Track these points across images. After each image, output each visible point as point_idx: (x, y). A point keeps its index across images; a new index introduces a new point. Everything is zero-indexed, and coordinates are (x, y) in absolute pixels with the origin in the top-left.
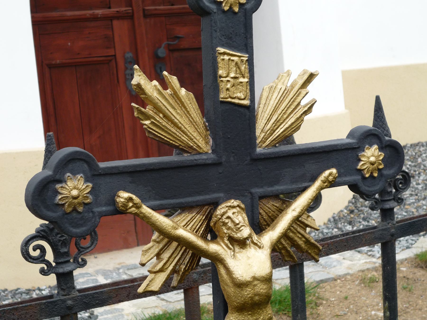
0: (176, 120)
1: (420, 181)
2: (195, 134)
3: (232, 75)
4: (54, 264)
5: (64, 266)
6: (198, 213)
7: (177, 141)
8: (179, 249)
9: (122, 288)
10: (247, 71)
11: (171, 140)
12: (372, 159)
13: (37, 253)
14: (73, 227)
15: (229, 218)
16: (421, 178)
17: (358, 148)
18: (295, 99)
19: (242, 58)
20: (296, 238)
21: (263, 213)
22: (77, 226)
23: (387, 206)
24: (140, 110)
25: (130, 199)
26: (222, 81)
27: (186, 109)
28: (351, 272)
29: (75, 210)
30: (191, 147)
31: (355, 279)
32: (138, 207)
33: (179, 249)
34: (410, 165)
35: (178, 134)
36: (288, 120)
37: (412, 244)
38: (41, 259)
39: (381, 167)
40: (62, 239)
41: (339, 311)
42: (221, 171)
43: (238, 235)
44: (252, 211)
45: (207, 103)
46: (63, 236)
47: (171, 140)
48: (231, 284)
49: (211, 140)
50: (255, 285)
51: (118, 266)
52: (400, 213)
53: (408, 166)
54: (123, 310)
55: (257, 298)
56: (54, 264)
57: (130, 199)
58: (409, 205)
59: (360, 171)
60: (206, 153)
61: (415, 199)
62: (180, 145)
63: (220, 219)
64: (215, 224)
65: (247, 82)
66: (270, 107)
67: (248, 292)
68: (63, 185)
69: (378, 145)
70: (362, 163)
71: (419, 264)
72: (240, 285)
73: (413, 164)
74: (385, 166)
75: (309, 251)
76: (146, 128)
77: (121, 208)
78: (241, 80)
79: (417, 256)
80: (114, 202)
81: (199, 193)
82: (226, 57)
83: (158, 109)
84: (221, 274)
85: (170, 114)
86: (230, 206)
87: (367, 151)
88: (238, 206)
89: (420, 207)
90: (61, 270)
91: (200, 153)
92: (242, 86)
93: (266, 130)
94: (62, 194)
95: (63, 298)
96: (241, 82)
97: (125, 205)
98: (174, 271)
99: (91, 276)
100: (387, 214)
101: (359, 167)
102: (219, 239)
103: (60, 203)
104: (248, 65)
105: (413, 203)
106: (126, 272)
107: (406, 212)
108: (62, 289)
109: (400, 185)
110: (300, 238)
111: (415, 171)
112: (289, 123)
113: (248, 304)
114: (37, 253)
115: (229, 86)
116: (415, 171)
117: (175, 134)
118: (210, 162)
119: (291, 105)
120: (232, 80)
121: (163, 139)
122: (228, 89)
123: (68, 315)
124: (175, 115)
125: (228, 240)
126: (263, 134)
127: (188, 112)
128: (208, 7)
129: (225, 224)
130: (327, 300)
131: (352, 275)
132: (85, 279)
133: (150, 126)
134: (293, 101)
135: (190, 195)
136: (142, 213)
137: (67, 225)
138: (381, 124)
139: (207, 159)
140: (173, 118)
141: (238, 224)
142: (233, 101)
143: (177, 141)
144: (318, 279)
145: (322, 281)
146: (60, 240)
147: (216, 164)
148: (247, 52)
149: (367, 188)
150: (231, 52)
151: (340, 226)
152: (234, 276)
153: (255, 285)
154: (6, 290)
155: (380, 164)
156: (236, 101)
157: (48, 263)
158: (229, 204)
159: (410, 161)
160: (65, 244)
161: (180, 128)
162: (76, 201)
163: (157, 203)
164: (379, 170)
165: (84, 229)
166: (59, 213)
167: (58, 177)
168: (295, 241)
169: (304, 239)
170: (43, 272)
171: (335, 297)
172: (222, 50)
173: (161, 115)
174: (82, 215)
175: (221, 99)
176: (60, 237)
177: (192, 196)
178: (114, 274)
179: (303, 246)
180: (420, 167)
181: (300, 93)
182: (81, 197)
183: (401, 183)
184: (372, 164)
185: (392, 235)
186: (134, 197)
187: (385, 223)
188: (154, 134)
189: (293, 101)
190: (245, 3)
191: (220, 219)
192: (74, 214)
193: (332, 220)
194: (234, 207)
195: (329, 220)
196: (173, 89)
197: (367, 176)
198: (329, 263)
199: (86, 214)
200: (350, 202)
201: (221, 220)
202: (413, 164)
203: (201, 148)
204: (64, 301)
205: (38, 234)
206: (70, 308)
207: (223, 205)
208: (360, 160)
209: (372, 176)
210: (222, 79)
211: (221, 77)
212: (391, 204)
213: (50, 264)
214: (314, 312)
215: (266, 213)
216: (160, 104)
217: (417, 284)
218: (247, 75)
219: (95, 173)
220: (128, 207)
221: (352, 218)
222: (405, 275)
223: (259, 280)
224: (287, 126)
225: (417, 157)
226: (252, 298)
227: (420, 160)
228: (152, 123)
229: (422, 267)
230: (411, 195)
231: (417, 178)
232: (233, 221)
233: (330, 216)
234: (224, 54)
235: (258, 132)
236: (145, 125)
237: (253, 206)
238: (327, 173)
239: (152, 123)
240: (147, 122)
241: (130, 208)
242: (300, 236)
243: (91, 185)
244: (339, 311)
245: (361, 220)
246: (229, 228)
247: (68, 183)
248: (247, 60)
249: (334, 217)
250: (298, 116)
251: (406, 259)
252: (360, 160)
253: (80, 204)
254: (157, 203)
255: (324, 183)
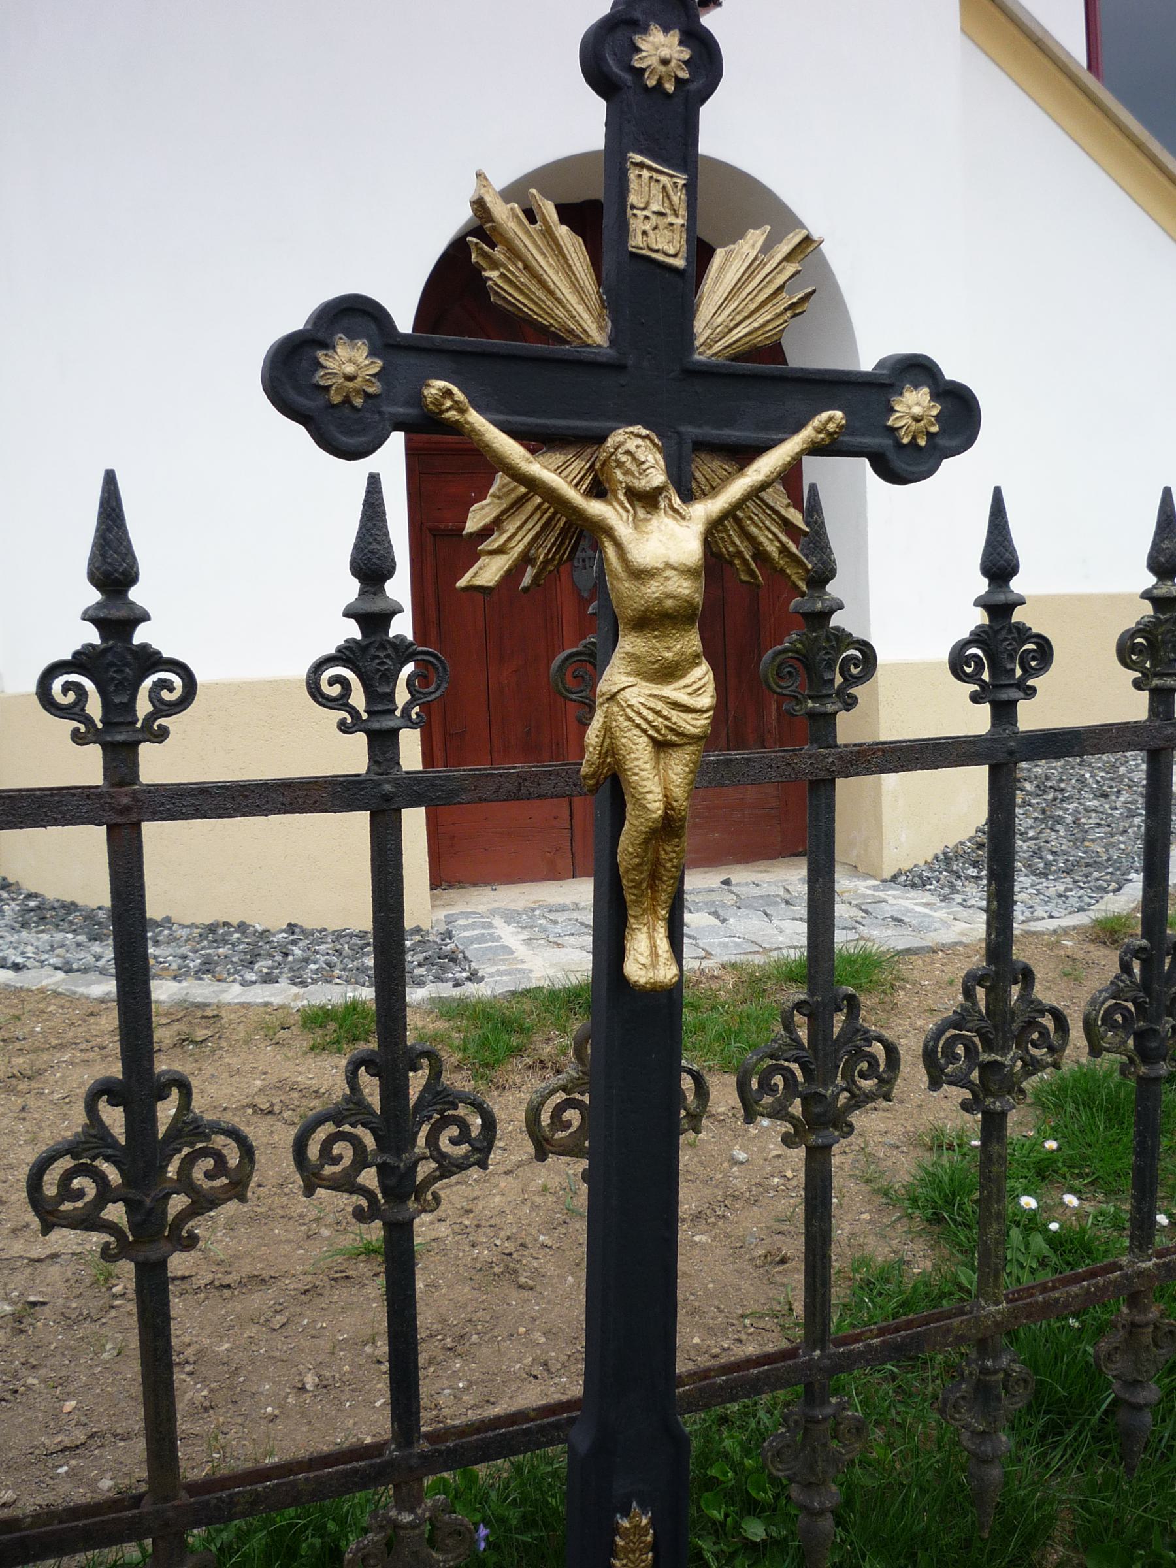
0: (545, 276)
1: (1118, 804)
2: (580, 309)
3: (655, 207)
4: (365, 716)
5: (382, 718)
6: (577, 456)
7: (546, 316)
8: (536, 518)
9: (487, 775)
10: (684, 205)
11: (536, 313)
12: (917, 410)
13: (335, 691)
14: (342, 432)
15: (628, 453)
16: (1122, 799)
17: (891, 385)
18: (774, 278)
19: (675, 180)
20: (763, 539)
21: (701, 479)
22: (350, 433)
23: (1005, 695)
24: (481, 249)
25: (448, 393)
26: (635, 215)
27: (564, 257)
28: (964, 940)
29: (347, 401)
30: (571, 332)
31: (971, 953)
32: (462, 411)
33: (536, 518)
34: (1102, 777)
35: (548, 303)
36: (757, 315)
37: (1089, 905)
38: (341, 702)
39: (935, 429)
40: (382, 668)
41: (935, 1003)
42: (622, 382)
43: (642, 484)
44: (679, 468)
45: (608, 259)
46: (385, 663)
47: (536, 313)
48: (623, 575)
49: (610, 324)
50: (667, 579)
51: (533, 905)
52: (1031, 716)
53: (1098, 778)
54: (531, 971)
55: (669, 603)
56: (365, 716)
57: (448, 393)
58: (1093, 841)
59: (893, 430)
60: (599, 346)
61: (1106, 833)
62: (551, 325)
63: (613, 454)
64: (604, 464)
65: (683, 225)
66: (724, 285)
67: (653, 589)
68: (330, 352)
69: (929, 387)
70: (898, 415)
71: (1098, 937)
72: (640, 575)
73: (1108, 776)
74: (943, 430)
75: (788, 571)
76: (491, 287)
77: (431, 406)
78: (671, 219)
79: (1097, 922)
80: (421, 397)
81: (579, 416)
82: (646, 174)
83: (515, 254)
84: (607, 560)
85: (535, 264)
86: (632, 433)
87: (907, 394)
88: (647, 437)
89: (1113, 845)
90: (376, 726)
91: (589, 346)
92: (673, 231)
93: (715, 325)
94: (326, 368)
95: (377, 777)
96: (671, 225)
97: (438, 403)
98: (525, 559)
99: (482, 917)
100: (1004, 712)
101: (890, 423)
102: (609, 495)
103: (322, 383)
104: (687, 195)
105: (1101, 838)
106: (547, 914)
107: (1084, 852)
108: (376, 762)
109: (1033, 664)
110: (771, 540)
111: (1111, 787)
112: (761, 321)
113: (652, 612)
114: (335, 691)
115: (647, 227)
116: (1111, 787)
117: (543, 302)
118: (604, 360)
119: (765, 287)
120: (653, 217)
121: (521, 310)
122: (644, 233)
123: (384, 811)
124: (546, 268)
125: (625, 494)
126: (709, 331)
127: (570, 266)
128: (617, 75)
129: (620, 464)
130: (914, 983)
131: (966, 946)
132: (471, 920)
133: (500, 282)
134: (770, 281)
135: (564, 417)
136: (468, 423)
137: (332, 428)
138: (1000, 539)
139: (598, 354)
140: (541, 272)
141: (643, 462)
142: (654, 255)
143: (546, 316)
144: (901, 946)
145: (908, 951)
146: (379, 670)
147: (616, 367)
148: (685, 171)
149: (904, 466)
150: (655, 165)
151: (955, 868)
152: (630, 557)
153: (667, 579)
154: (325, 930)
155: (933, 425)
156: (660, 257)
157: (353, 712)
158: (631, 429)
159: (1104, 770)
160: (388, 678)
161: (552, 293)
162: (350, 384)
163: (501, 417)
164: (930, 435)
165: (362, 439)
166: (320, 403)
167: (321, 335)
168: (761, 543)
169: (777, 544)
170: (344, 727)
171: (930, 980)
172: (638, 158)
173: (520, 265)
174: (361, 414)
175: (630, 249)
176: (378, 664)
177: (566, 418)
178: (524, 916)
179: (776, 555)
180: (1122, 781)
181: (784, 268)
182: (359, 379)
183: (1034, 659)
184: (917, 419)
185: (1011, 753)
186: (455, 390)
187: (999, 729)
188: (504, 298)
189: (770, 281)
190: (687, 80)
191: (613, 454)
192: (347, 411)
193: (942, 857)
194: (639, 436)
195: (936, 858)
196: (545, 221)
197: (905, 441)
198: (926, 924)
199: (368, 415)
200: (978, 830)
201: (613, 457)
202: (1108, 776)
203: (589, 336)
204: (377, 784)
205: (339, 654)
206: (387, 798)
207: (620, 431)
208: (893, 410)
209: (913, 442)
210: (635, 211)
211: (633, 207)
212: (1013, 694)
213: (358, 712)
214: (887, 999)
215: (707, 480)
216: (517, 242)
217: (1091, 971)
218: (683, 212)
219: (391, 342)
220: (444, 407)
221: (979, 856)
222: (1070, 954)
223: (675, 569)
224: (756, 325)
225: (1118, 764)
226: (660, 601)
227: (1122, 770)
228: (502, 275)
229: (1105, 943)
230: (1099, 825)
231: (1113, 798)
232: (634, 459)
233: (938, 850)
234: (641, 165)
235: (699, 325)
236: (490, 279)
237: (680, 457)
238: (825, 416)
239: (502, 275)
240: (494, 274)
241: (447, 410)
242: (770, 536)
243: (380, 363)
244: (935, 1003)
245: (1089, 1151)
246: (627, 472)
247: (339, 350)
248: (684, 185)
249: (945, 853)
250: (778, 311)
251: (1075, 928)
252: (893, 410)
253: (357, 391)
254: (501, 417)
255: (819, 432)
